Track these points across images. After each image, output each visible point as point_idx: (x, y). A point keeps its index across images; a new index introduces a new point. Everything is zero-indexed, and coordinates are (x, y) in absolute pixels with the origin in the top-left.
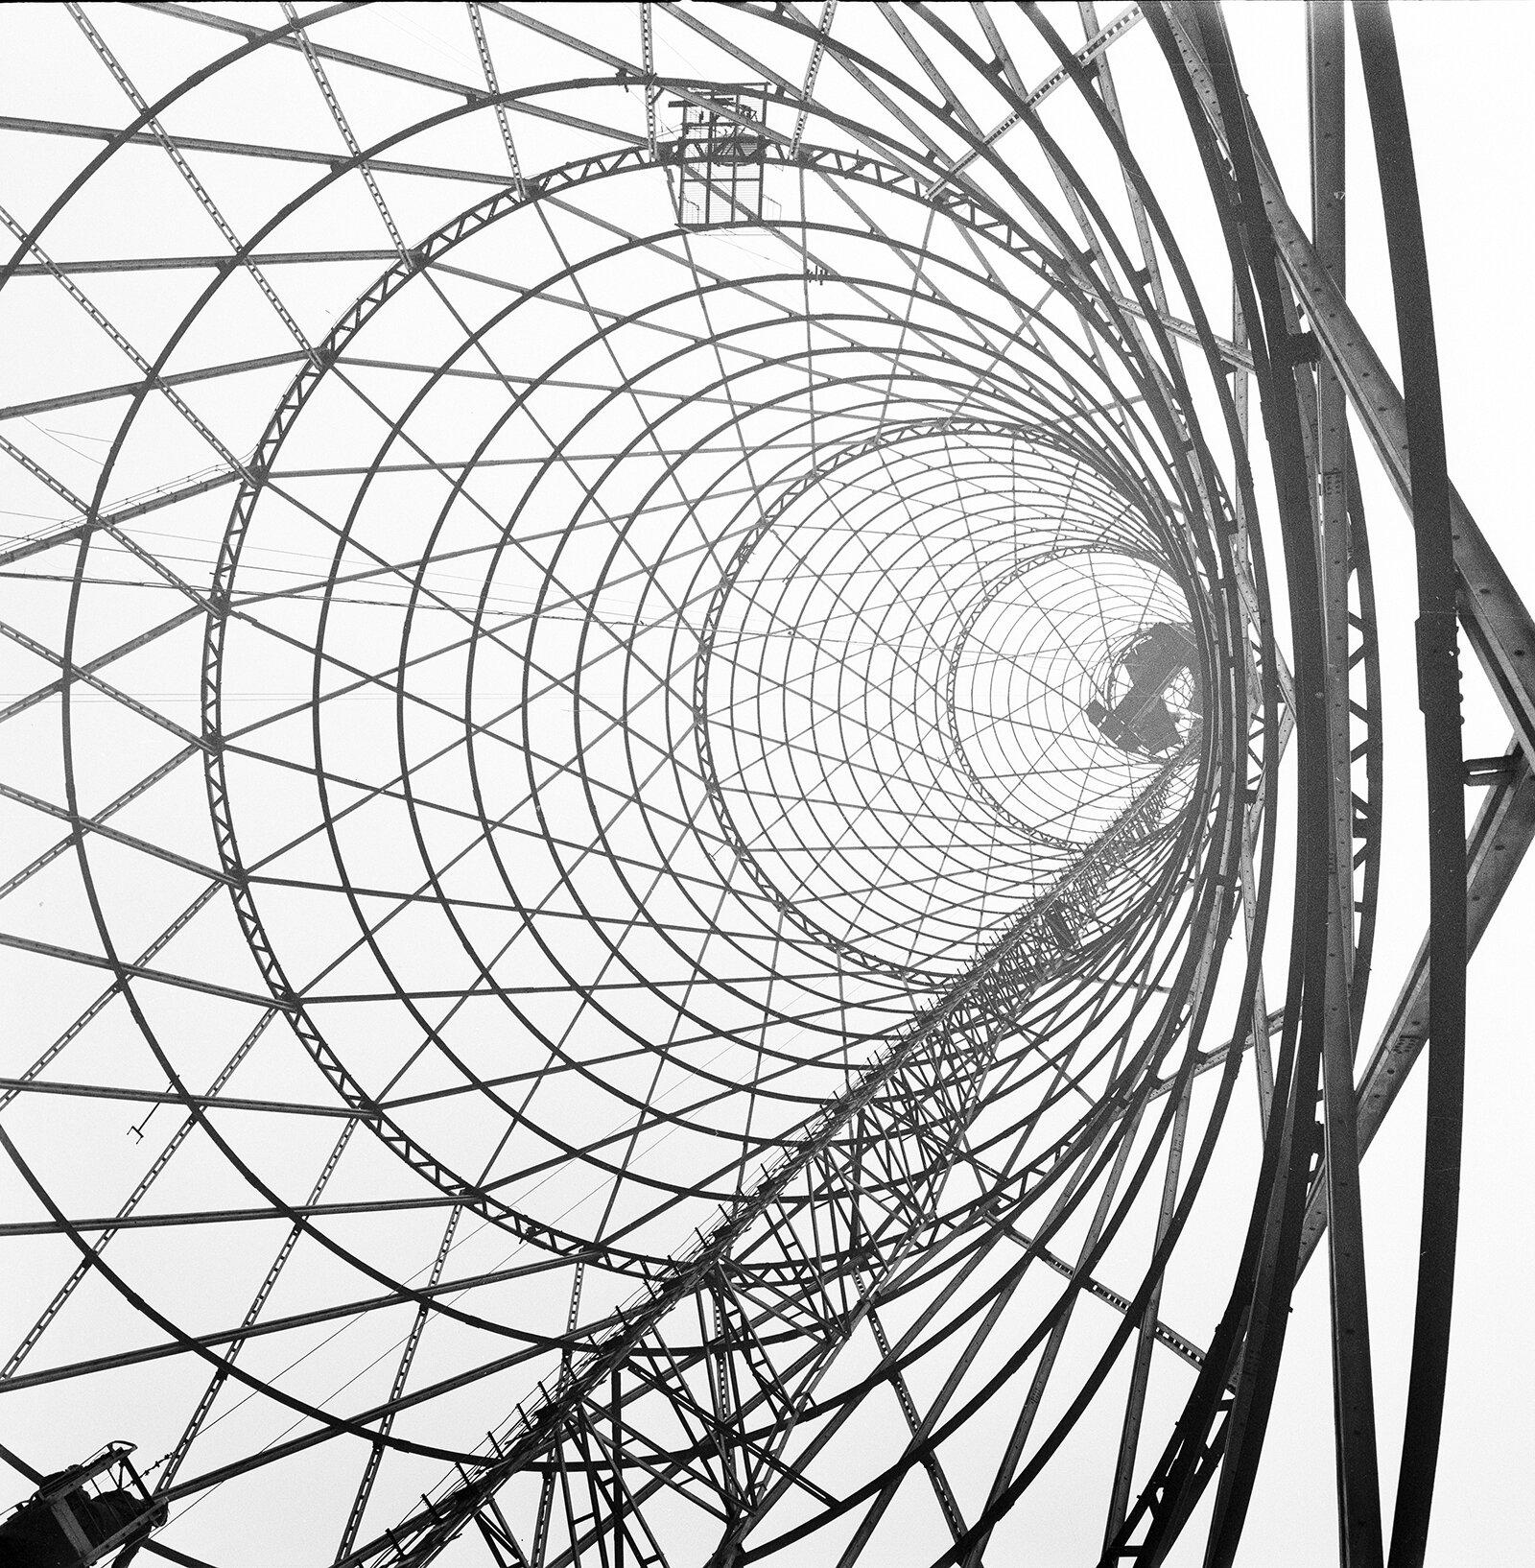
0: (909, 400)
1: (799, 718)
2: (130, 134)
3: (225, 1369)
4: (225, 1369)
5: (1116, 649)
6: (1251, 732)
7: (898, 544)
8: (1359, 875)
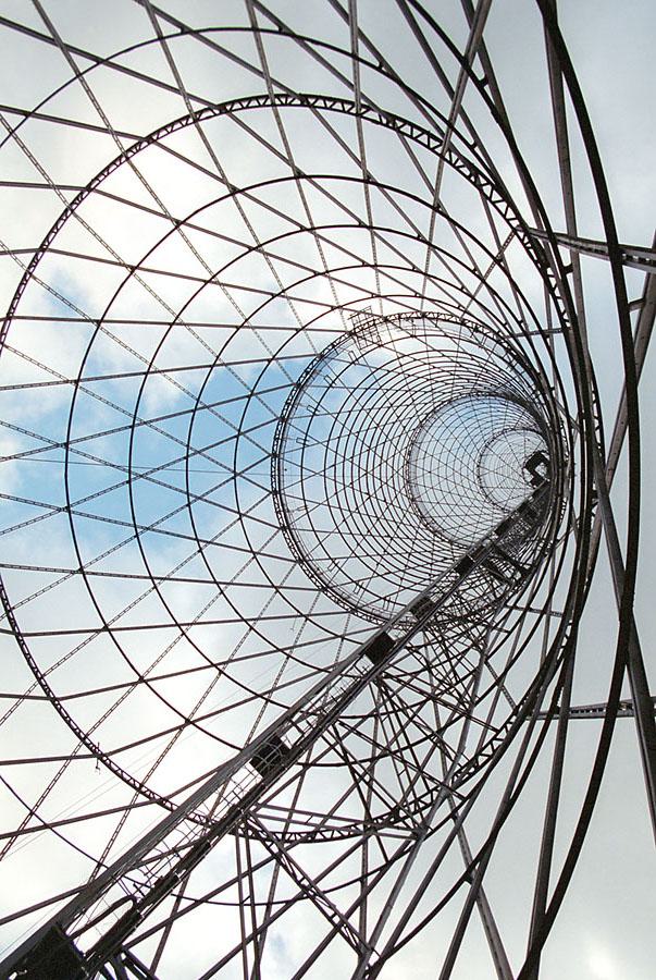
0: (509, 275)
1: (435, 465)
2: (210, 281)
3: (289, 656)
4: (289, 656)
5: (522, 463)
6: (501, 743)
7: (450, 442)
8: (598, 432)
